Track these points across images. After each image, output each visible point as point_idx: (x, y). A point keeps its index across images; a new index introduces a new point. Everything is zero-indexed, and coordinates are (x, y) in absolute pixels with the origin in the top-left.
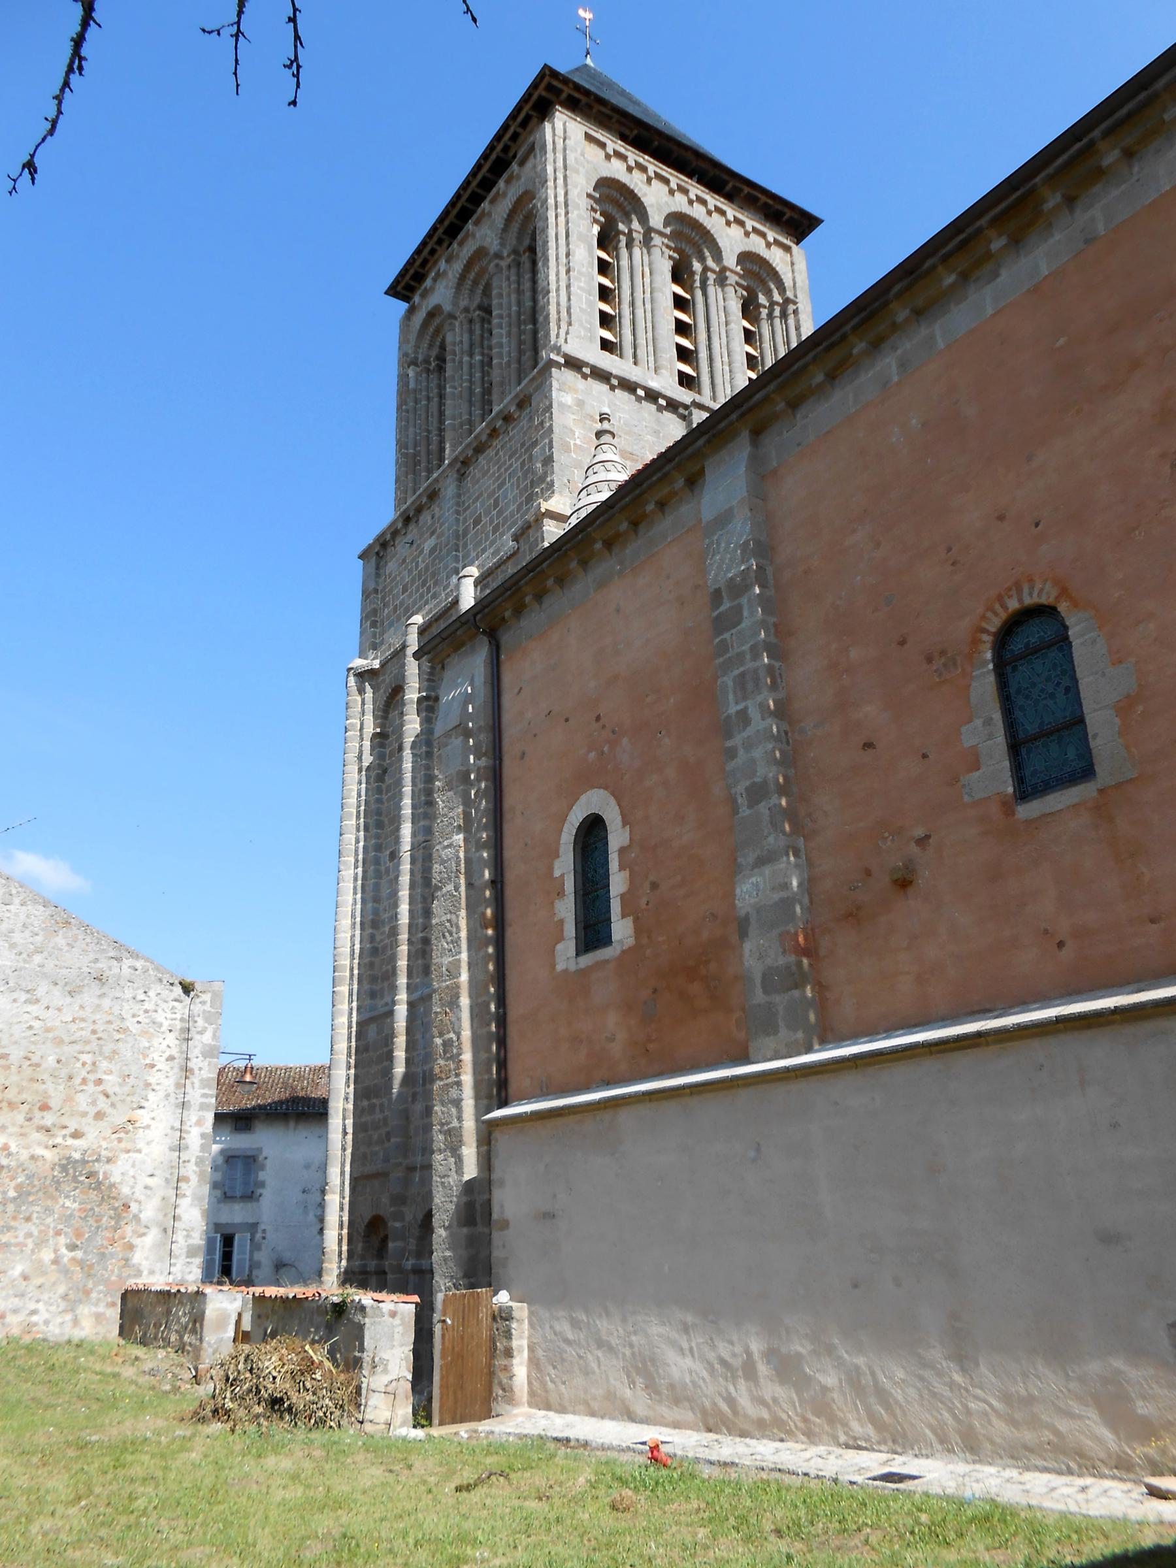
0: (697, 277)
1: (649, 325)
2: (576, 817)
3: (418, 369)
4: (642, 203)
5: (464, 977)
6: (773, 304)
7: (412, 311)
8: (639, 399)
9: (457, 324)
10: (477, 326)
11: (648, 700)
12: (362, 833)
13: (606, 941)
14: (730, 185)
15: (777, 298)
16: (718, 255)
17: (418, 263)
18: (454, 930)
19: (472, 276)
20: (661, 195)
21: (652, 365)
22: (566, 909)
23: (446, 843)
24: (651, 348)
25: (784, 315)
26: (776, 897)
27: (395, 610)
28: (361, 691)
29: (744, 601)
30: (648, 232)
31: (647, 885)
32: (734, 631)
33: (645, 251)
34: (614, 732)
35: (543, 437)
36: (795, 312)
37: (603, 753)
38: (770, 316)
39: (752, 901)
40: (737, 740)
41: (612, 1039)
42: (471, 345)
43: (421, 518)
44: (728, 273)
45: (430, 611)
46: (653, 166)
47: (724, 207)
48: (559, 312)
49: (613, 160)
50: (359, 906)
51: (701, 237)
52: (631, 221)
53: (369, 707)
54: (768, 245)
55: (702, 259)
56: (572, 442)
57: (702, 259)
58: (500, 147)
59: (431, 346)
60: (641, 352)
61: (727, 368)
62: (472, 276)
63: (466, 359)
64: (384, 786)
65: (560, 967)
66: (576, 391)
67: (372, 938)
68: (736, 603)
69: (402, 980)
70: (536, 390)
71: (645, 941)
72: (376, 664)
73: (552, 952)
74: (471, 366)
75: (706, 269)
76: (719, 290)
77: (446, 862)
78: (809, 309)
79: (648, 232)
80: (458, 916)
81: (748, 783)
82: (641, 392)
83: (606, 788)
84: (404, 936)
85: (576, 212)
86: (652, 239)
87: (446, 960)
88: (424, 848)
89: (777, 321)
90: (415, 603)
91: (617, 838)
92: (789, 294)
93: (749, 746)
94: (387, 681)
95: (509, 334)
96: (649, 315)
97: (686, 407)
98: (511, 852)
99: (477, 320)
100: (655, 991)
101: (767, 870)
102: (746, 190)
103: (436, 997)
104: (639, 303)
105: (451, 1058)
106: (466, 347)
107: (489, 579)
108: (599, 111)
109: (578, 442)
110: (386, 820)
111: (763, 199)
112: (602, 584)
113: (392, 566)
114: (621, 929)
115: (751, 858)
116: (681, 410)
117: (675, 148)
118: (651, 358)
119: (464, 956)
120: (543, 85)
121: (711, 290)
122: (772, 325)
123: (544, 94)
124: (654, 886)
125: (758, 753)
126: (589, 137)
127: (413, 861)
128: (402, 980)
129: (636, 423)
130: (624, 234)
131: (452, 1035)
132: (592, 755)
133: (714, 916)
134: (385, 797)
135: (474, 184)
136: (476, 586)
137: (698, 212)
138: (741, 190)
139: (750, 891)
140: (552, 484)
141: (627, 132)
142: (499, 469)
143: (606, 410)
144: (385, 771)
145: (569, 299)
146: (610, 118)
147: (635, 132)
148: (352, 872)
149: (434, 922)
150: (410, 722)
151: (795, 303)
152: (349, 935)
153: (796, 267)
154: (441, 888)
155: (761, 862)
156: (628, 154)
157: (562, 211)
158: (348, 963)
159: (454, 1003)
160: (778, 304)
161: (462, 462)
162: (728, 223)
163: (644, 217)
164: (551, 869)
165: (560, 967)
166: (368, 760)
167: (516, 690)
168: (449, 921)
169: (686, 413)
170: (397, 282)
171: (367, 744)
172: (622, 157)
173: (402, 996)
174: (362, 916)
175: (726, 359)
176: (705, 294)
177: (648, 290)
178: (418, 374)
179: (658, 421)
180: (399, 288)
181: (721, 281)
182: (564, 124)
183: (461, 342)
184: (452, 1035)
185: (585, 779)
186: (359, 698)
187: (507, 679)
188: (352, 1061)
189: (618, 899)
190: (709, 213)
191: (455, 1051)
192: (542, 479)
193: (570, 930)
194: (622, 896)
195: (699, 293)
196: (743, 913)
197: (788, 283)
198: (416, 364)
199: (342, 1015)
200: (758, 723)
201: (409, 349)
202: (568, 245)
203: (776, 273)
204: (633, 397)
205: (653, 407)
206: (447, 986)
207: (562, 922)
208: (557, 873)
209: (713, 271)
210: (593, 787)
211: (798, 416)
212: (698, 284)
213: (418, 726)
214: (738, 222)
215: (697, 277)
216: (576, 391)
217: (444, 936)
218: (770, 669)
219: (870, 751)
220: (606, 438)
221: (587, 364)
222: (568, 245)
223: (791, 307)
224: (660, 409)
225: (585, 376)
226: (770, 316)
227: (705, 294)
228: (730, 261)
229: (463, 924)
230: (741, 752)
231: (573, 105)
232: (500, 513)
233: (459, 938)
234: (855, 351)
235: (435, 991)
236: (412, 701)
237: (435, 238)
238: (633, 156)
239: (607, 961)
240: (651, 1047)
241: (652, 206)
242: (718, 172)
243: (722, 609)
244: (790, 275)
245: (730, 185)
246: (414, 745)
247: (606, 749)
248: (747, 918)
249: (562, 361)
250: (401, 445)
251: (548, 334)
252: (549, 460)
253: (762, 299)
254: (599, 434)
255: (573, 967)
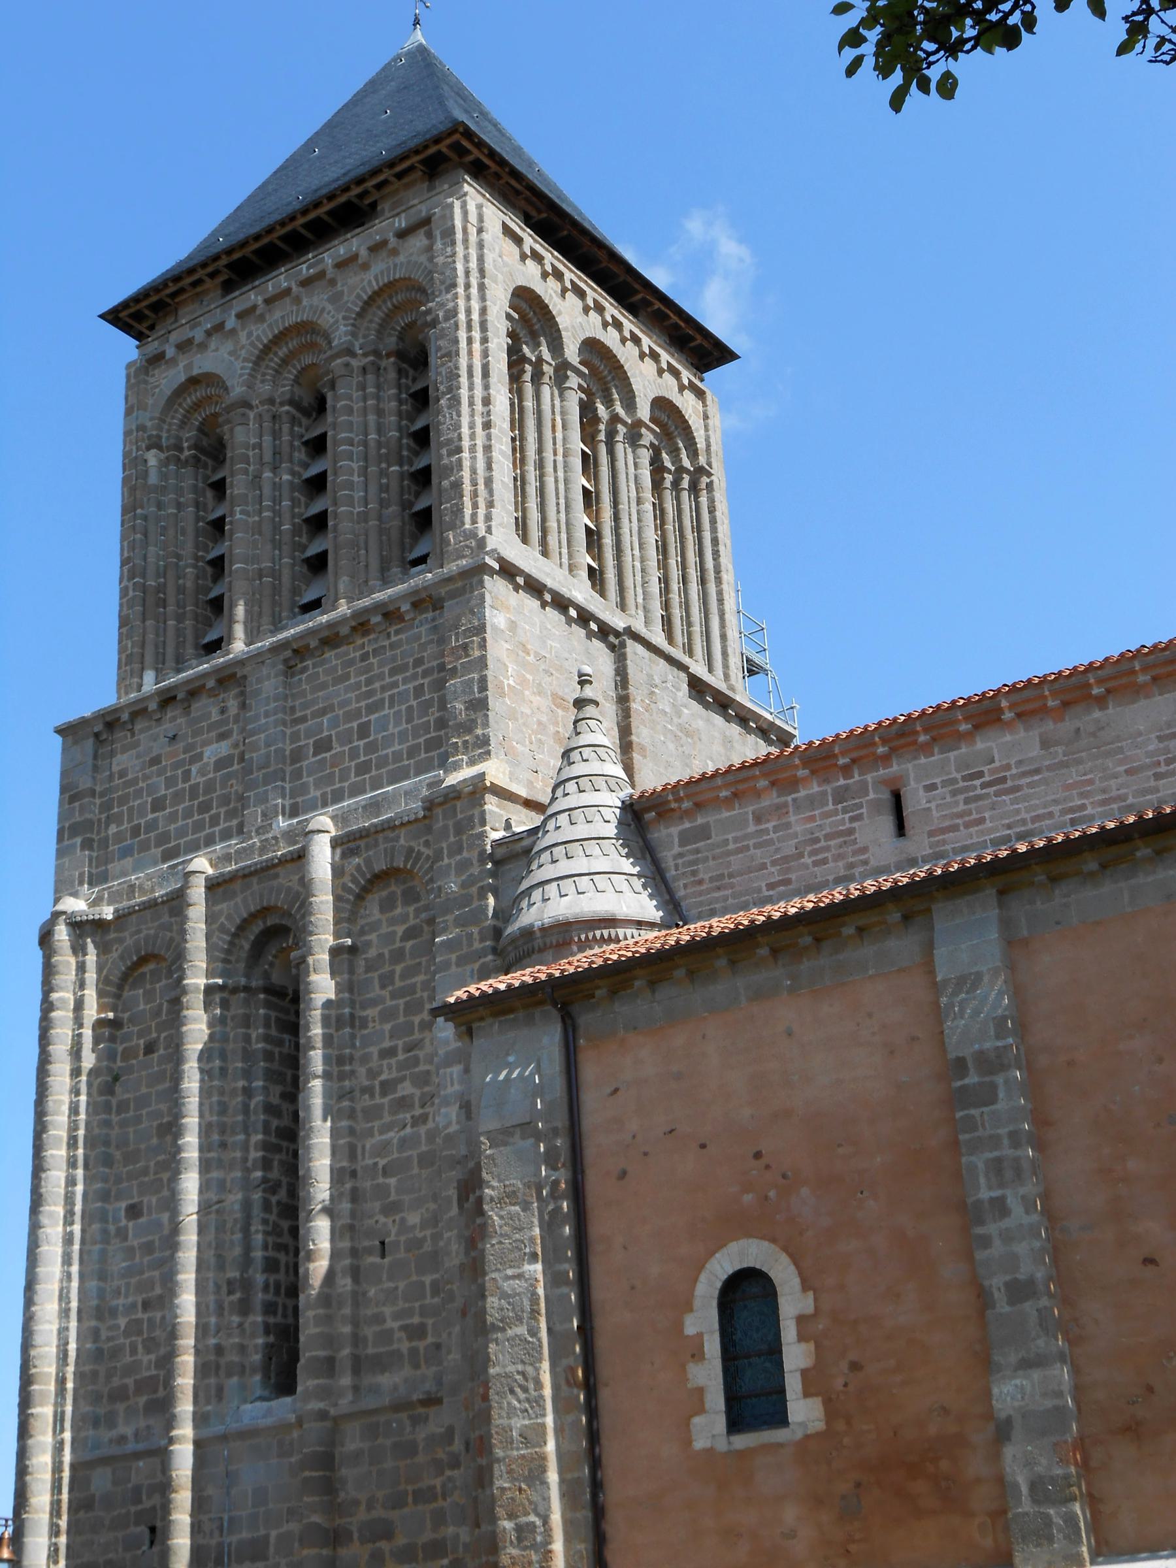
0: (602, 427)
1: (562, 501)
2: (723, 1265)
3: (163, 456)
4: (556, 324)
5: (551, 1446)
6: (680, 470)
7: (155, 360)
8: (569, 621)
9: (252, 415)
10: (286, 428)
11: (841, 1151)
12: (80, 1173)
13: (779, 1418)
14: (639, 296)
15: (686, 463)
16: (630, 402)
17: (169, 291)
18: (531, 1386)
19: (283, 352)
20: (580, 315)
21: (565, 560)
22: (709, 1375)
23: (510, 1272)
24: (564, 536)
25: (694, 488)
26: (1049, 1403)
27: (136, 831)
28: (78, 949)
29: (999, 1079)
30: (563, 367)
31: (844, 1365)
32: (986, 1109)
33: (556, 392)
34: (784, 1176)
35: (468, 668)
36: (710, 486)
37: (766, 1198)
38: (676, 484)
39: (1016, 1404)
40: (991, 1228)
41: (792, 1535)
42: (276, 453)
43: (195, 706)
44: (643, 430)
45: (227, 858)
46: (571, 274)
47: (640, 335)
48: (474, 483)
49: (529, 261)
50: (75, 1284)
51: (610, 372)
52: (539, 345)
53: (91, 976)
54: (682, 388)
55: (609, 403)
56: (506, 682)
57: (609, 403)
58: (356, 191)
59: (183, 424)
60: (552, 540)
61: (638, 564)
62: (283, 352)
63: (267, 474)
64: (114, 1102)
65: (699, 1444)
66: (508, 608)
67: (95, 1334)
68: (987, 1079)
69: (185, 1407)
70: (453, 595)
71: (840, 1426)
72: (108, 912)
73: (685, 1424)
74: (276, 487)
75: (615, 419)
76: (629, 450)
77: (509, 1296)
78: (724, 485)
79: (563, 367)
80: (537, 1370)
81: (1008, 1278)
82: (573, 613)
83: (773, 1240)
84: (188, 1341)
85: (496, 340)
86: (567, 377)
87: (518, 1423)
88: (218, 1211)
89: (685, 494)
90: (181, 832)
91: (792, 1304)
92: (702, 460)
93: (1007, 1237)
94: (129, 942)
95: (364, 472)
96: (562, 486)
97: (617, 634)
98: (599, 1294)
99: (285, 418)
100: (858, 1485)
101: (1036, 1374)
102: (658, 305)
103: (498, 1469)
104: (549, 469)
105: (534, 1546)
106: (268, 456)
107: (362, 843)
108: (507, 183)
109: (511, 682)
110: (118, 1155)
111: (699, 340)
112: (759, 995)
113: (124, 760)
114: (803, 1412)
115: (1013, 1358)
116: (612, 638)
117: (585, 241)
118: (565, 551)
119: (549, 1420)
120: (448, 141)
121: (620, 448)
122: (678, 499)
123: (444, 150)
124: (855, 1366)
125: (1021, 1248)
126: (507, 231)
127: (202, 1229)
128: (185, 1407)
129: (566, 655)
130: (530, 362)
131: (532, 1518)
132: (748, 1198)
133: (945, 1411)
134: (115, 1119)
135: (302, 220)
136: (333, 847)
137: (611, 339)
138: (651, 304)
139: (1010, 1393)
140: (485, 741)
141: (533, 213)
142: (369, 682)
143: (587, 669)
144: (116, 1079)
145: (489, 467)
146: (518, 193)
147: (544, 215)
148: (60, 1229)
149: (492, 1371)
150: (195, 1020)
151: (709, 475)
152: (55, 1327)
153: (710, 422)
154: (503, 1330)
155: (1026, 1365)
156: (588, 290)
157: (476, 334)
158: (52, 1370)
159: (536, 1474)
160: (687, 471)
161: (295, 651)
162: (642, 356)
163: (556, 345)
164: (679, 1326)
165: (699, 1444)
166: (89, 1060)
167: (609, 1090)
168: (523, 1374)
169: (616, 642)
170: (125, 305)
171: (87, 1033)
172: (537, 257)
173: (185, 1431)
174: (80, 1300)
175: (637, 552)
176: (611, 452)
177: (560, 451)
178: (165, 463)
179: (587, 652)
180: (122, 315)
181: (634, 439)
182: (480, 207)
183: (259, 446)
184: (532, 1518)
185: (737, 1224)
186: (72, 960)
187: (589, 1071)
188: (63, 1523)
189: (798, 1375)
190: (623, 341)
191: (539, 1539)
192: (468, 727)
193: (716, 1399)
194: (804, 1373)
195: (603, 449)
196: (1003, 1415)
197: (701, 445)
198: (159, 448)
199: (44, 1452)
200: (1018, 1215)
201: (147, 418)
202: (486, 387)
203: (626, 378)
204: (563, 618)
205: (582, 632)
206: (523, 1456)
207: (700, 1391)
208: (690, 1330)
209: (625, 424)
210: (748, 1235)
211: (1057, 892)
212: (602, 436)
213: (204, 1027)
214: (655, 356)
215: (602, 427)
216: (508, 608)
217: (512, 1391)
218: (1033, 1161)
219: (1150, 1267)
220: (590, 710)
221: (521, 572)
222: (486, 387)
223: (705, 480)
224: (590, 635)
225: (517, 587)
226: (676, 484)
227: (611, 452)
228: (572, 352)
229: (546, 1378)
230: (997, 1242)
231: (478, 172)
232: (371, 748)
233: (542, 1397)
234: (1138, 854)
235: (498, 1461)
236: (197, 986)
237: (210, 269)
238: (551, 258)
239: (780, 1445)
240: (853, 1548)
241: (566, 329)
242: (629, 279)
243: (967, 1081)
244: (702, 432)
245: (639, 296)
246: (205, 1056)
247: (772, 1194)
248: (1009, 1421)
249: (496, 566)
250: (132, 568)
251: (458, 511)
252: (480, 705)
253: (602, 410)
254: (580, 703)
255: (722, 1445)
